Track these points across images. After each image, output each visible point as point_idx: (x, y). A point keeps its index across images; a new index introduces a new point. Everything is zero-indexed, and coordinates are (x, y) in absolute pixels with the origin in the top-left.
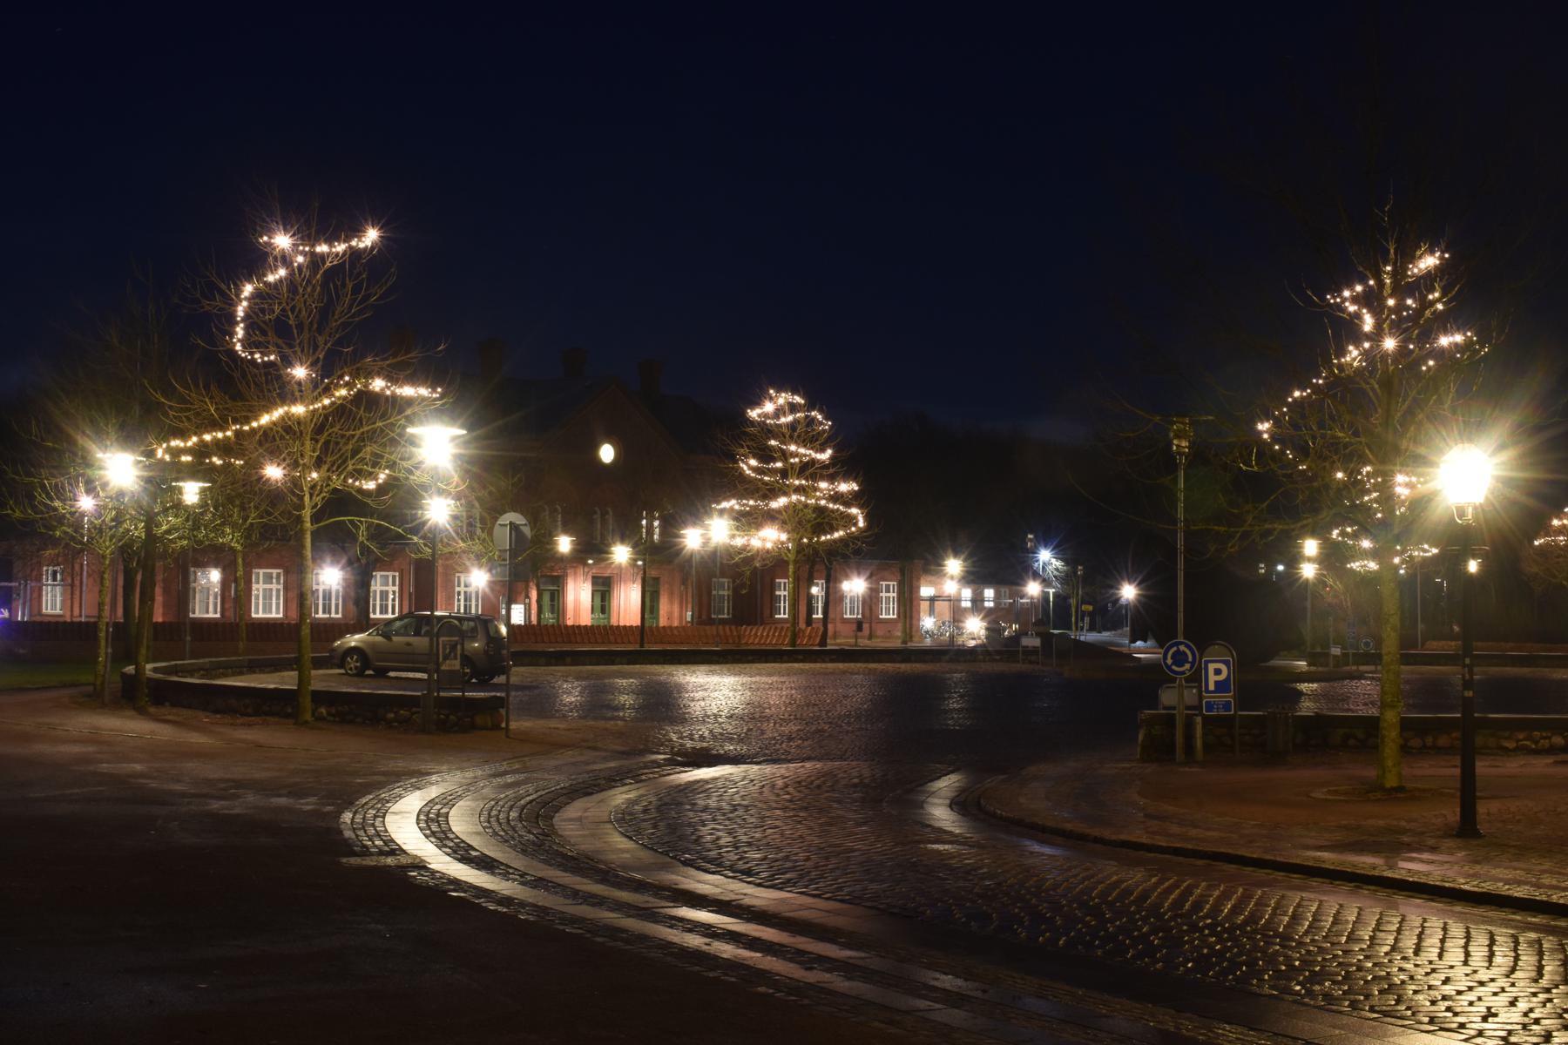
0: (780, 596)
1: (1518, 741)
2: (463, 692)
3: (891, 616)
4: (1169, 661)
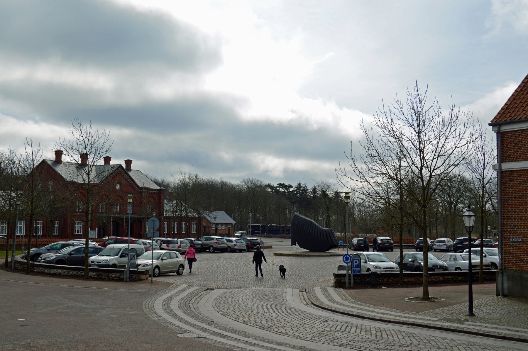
0: (39, 227)
1: (432, 279)
2: (280, 225)
3: (80, 234)
4: (349, 261)
